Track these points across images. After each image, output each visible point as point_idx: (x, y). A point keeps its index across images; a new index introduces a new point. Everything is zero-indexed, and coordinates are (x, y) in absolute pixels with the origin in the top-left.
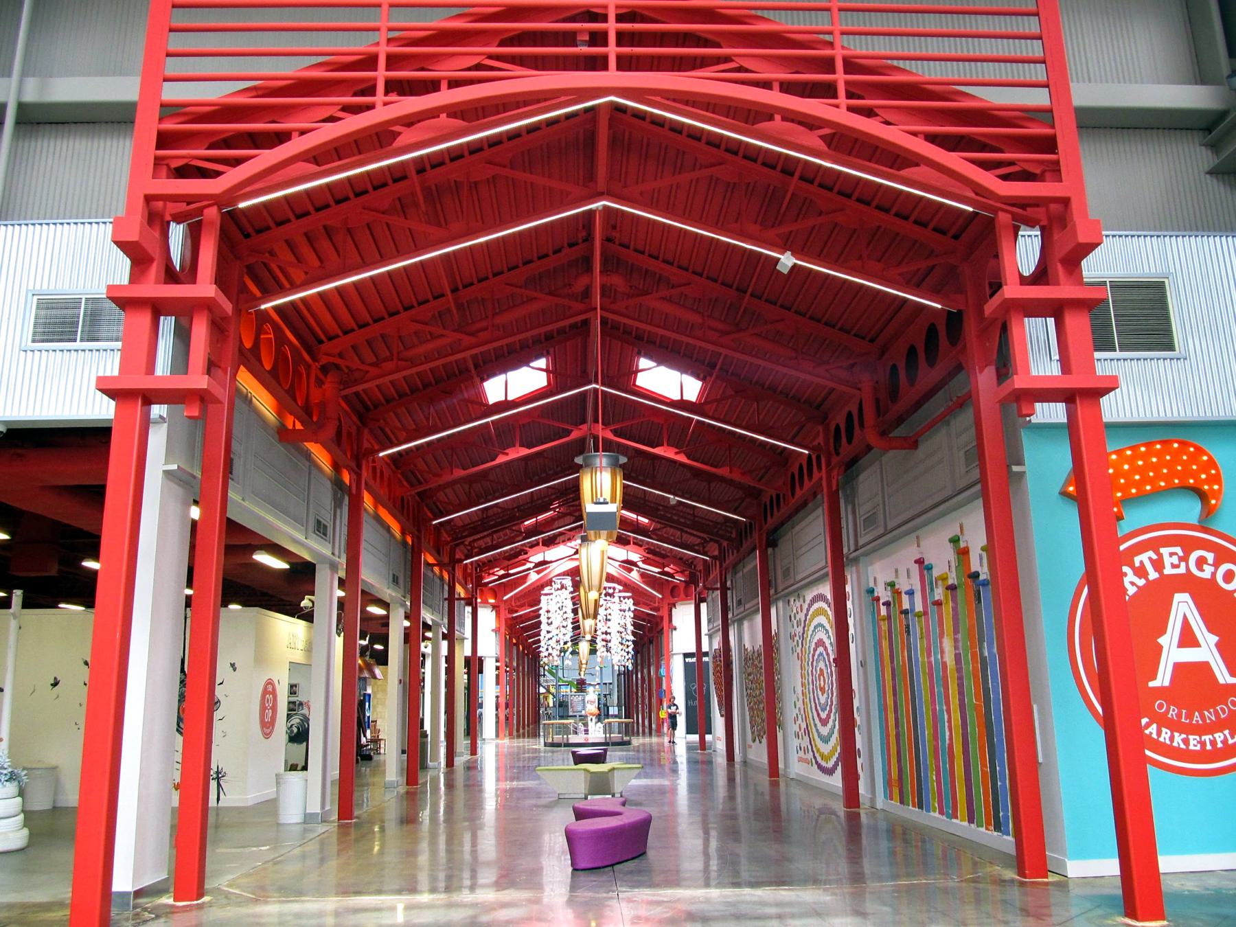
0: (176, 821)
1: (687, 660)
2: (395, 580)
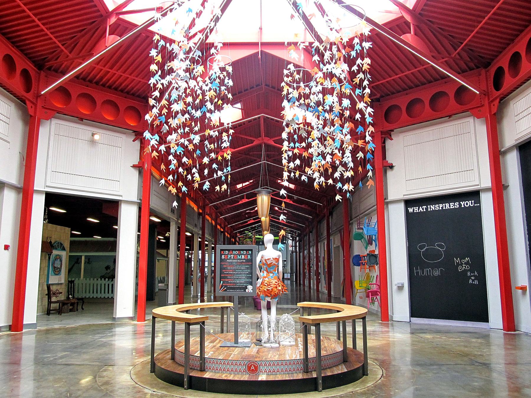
0: (504, 192)
1: (411, 210)
2: (210, 235)
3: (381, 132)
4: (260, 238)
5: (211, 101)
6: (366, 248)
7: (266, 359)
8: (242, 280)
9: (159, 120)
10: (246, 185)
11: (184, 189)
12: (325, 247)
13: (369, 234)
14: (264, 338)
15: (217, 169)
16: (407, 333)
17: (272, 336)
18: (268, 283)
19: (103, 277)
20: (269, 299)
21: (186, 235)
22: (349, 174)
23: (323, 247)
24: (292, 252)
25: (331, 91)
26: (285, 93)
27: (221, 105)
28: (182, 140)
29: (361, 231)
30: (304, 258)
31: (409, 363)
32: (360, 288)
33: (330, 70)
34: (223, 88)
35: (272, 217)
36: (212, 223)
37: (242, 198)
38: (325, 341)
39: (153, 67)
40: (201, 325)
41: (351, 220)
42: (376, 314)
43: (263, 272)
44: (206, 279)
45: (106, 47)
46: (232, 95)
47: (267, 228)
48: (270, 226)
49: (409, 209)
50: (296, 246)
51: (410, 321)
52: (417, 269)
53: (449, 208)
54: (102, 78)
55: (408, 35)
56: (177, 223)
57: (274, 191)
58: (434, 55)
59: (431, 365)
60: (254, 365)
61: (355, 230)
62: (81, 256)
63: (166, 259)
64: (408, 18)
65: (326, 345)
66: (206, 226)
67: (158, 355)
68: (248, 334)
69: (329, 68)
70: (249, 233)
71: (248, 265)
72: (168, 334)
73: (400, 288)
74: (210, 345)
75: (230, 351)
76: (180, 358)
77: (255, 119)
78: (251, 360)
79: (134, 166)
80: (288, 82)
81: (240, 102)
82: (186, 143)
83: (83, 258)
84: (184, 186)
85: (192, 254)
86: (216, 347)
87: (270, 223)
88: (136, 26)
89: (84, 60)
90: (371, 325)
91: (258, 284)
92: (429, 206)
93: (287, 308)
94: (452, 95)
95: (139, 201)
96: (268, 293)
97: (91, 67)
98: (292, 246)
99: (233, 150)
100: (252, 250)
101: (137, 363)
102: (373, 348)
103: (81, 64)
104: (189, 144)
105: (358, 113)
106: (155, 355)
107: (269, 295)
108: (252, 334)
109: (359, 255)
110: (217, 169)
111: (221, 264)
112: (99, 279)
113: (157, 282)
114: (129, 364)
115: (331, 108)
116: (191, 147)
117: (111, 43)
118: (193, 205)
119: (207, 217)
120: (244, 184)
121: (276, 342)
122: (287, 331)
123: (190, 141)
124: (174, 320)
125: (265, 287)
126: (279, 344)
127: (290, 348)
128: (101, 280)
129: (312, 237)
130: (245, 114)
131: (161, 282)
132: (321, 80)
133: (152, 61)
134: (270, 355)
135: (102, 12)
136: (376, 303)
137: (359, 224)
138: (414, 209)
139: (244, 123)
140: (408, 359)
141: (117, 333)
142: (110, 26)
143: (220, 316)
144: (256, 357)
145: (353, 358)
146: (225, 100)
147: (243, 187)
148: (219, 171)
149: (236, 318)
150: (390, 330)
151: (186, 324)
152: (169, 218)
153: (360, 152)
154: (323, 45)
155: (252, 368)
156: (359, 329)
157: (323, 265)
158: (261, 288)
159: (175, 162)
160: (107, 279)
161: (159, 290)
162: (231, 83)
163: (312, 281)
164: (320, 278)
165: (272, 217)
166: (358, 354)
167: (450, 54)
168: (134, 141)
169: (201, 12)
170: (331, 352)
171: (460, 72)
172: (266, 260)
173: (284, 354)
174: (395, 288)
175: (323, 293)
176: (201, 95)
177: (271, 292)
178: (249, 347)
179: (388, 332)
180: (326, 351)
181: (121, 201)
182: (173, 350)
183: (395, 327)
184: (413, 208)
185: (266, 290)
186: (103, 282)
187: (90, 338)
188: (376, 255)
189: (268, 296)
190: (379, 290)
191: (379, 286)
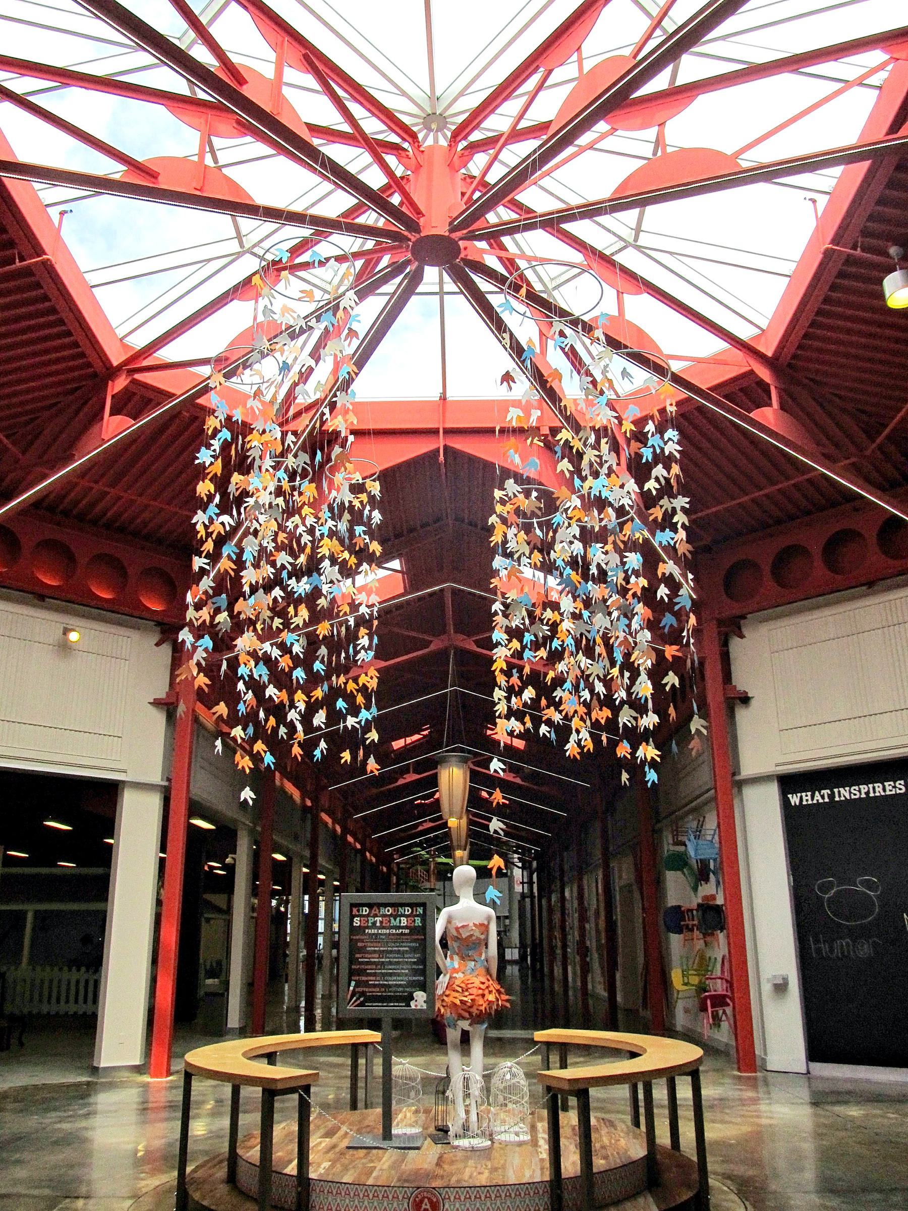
1: (794, 799)
3: (718, 620)
4: (447, 864)
5: (333, 561)
6: (695, 889)
7: (458, 1181)
8: (400, 978)
9: (214, 603)
10: (413, 742)
11: (269, 759)
12: (600, 885)
13: (702, 857)
14: (454, 1128)
15: (344, 711)
16: (802, 1104)
17: (473, 1117)
18: (463, 985)
19: (75, 963)
20: (465, 1025)
21: (274, 859)
22: (650, 720)
23: (593, 885)
24: (523, 896)
25: (602, 536)
26: (497, 538)
27: (354, 567)
28: (267, 647)
29: (682, 848)
30: (550, 910)
31: (811, 1187)
32: (686, 988)
33: (595, 492)
34: (359, 529)
35: (475, 815)
36: (335, 830)
37: (405, 770)
38: (604, 1131)
39: (204, 488)
40: (300, 1095)
41: (658, 821)
42: (727, 1054)
43: (452, 958)
44: (320, 963)
45: (104, 441)
46: (381, 543)
47: (463, 843)
48: (468, 836)
49: (790, 796)
50: (530, 883)
51: (808, 1072)
52: (817, 941)
53: (883, 794)
54: (93, 505)
55: (766, 410)
56: (252, 832)
57: (476, 754)
58: (826, 451)
59: (864, 1190)
60: (429, 1199)
61: (668, 847)
62: (25, 913)
63: (227, 917)
64: (764, 374)
65: (606, 1140)
66: (321, 838)
67: (194, 1171)
68: (417, 1112)
69: (596, 486)
70: (423, 852)
71: (415, 941)
72: (223, 1109)
73: (781, 988)
74: (323, 1145)
75: (372, 1161)
76: (249, 1179)
77: (431, 595)
78: (422, 1184)
79: (157, 703)
80: (505, 515)
81: (399, 556)
82: (275, 653)
83: (30, 917)
84: (268, 753)
85: (287, 902)
86: (337, 1150)
87: (469, 830)
88: (170, 396)
89: (54, 466)
90: (715, 1083)
91: (439, 987)
92: (836, 790)
93: (513, 1039)
94: (871, 536)
95: (165, 783)
96: (465, 1011)
97: (68, 484)
98: (523, 883)
99: (383, 664)
100: (424, 905)
101: (144, 1190)
102: (721, 1144)
103: (45, 477)
104: (281, 656)
105: (663, 585)
106: (189, 1169)
107: (467, 1015)
108: (427, 1111)
109: (679, 907)
110: (344, 711)
111: (351, 940)
112: (66, 968)
113: (202, 974)
114: (125, 1192)
115: (603, 574)
116: (285, 663)
117: (117, 428)
118: (290, 788)
119: (324, 816)
120: (409, 740)
121: (483, 1133)
122: (510, 1106)
123: (285, 649)
124: (237, 1082)
125: (457, 994)
126: (491, 1137)
127: (517, 1149)
128: (70, 970)
129: (569, 859)
130: (411, 585)
131: (212, 974)
132: (578, 514)
133: (200, 472)
134: (468, 1171)
135: (98, 365)
136: (725, 1025)
137: (676, 833)
138: (801, 797)
139: (408, 602)
140: (809, 1175)
141: (99, 1107)
142: (113, 396)
143: (349, 1062)
144: (435, 1177)
145: (671, 1176)
146: (363, 555)
147: (406, 745)
148: (349, 717)
149: (387, 1066)
150: (761, 1095)
151: (266, 1093)
152: (235, 821)
153: (671, 673)
154: (579, 437)
155: (424, 1206)
156: (684, 1092)
157: (595, 927)
158: (445, 998)
159: (250, 696)
160: (83, 969)
161: (207, 994)
162: (377, 516)
163: (570, 968)
164: (588, 959)
165: (475, 815)
166: (683, 1164)
167: (860, 449)
168: (157, 645)
169: (311, 370)
170: (618, 1161)
171: (885, 487)
172: (457, 929)
173: (504, 1167)
174: (767, 988)
175: (596, 997)
176: (309, 544)
177: (471, 1007)
178: (418, 1148)
179: (755, 1101)
180: (605, 1158)
181: (123, 782)
182: (233, 1158)
183: (772, 1088)
184: (799, 795)
185: (458, 1002)
186: (74, 975)
187: (32, 1122)
188: (718, 906)
189: (464, 1018)
190: (729, 994)
191: (730, 983)
